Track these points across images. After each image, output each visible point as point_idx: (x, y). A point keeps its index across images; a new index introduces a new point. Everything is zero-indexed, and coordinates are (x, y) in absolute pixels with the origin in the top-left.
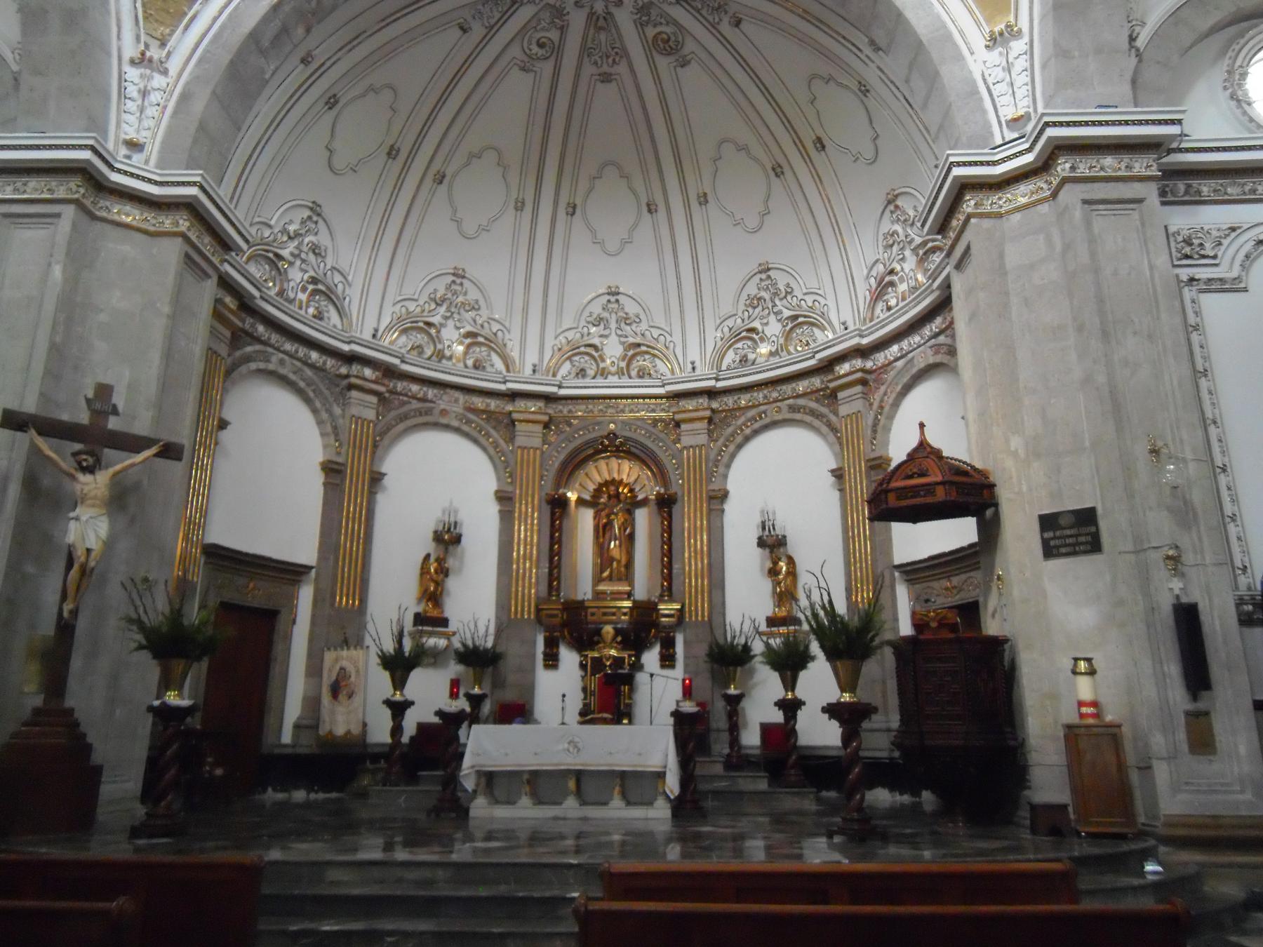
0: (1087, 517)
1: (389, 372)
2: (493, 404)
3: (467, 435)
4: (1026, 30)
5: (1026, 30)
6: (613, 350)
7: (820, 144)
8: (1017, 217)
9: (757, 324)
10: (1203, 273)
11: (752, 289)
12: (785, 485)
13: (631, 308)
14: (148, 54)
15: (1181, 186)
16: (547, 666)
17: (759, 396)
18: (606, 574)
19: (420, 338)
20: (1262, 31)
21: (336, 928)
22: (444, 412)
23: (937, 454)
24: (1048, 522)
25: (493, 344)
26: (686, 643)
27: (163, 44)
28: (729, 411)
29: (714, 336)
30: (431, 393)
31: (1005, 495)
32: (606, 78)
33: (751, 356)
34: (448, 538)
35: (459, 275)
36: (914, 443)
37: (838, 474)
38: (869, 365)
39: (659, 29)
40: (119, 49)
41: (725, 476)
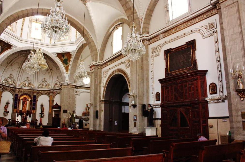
0: (66, 110)
1: (3, 86)
2: (13, 89)
3: (10, 92)
6: (27, 84)
7: (52, 70)
8: (65, 88)
9: (43, 84)
10: (77, 94)
11: (43, 80)
12: (43, 100)
13: (29, 79)
15: (77, 87)
16: (17, 117)
17: (42, 91)
18: (24, 108)
19: (6, 81)
22: (8, 90)
23: (57, 104)
24: (64, 110)
25: (14, 82)
26: (32, 115)
28: (40, 92)
29: (38, 84)
30: (7, 87)
31: (62, 108)
33: (42, 87)
34: (8, 103)
35: (11, 74)
36: (56, 103)
37: (49, 101)
38: (54, 91)
41: (38, 99)
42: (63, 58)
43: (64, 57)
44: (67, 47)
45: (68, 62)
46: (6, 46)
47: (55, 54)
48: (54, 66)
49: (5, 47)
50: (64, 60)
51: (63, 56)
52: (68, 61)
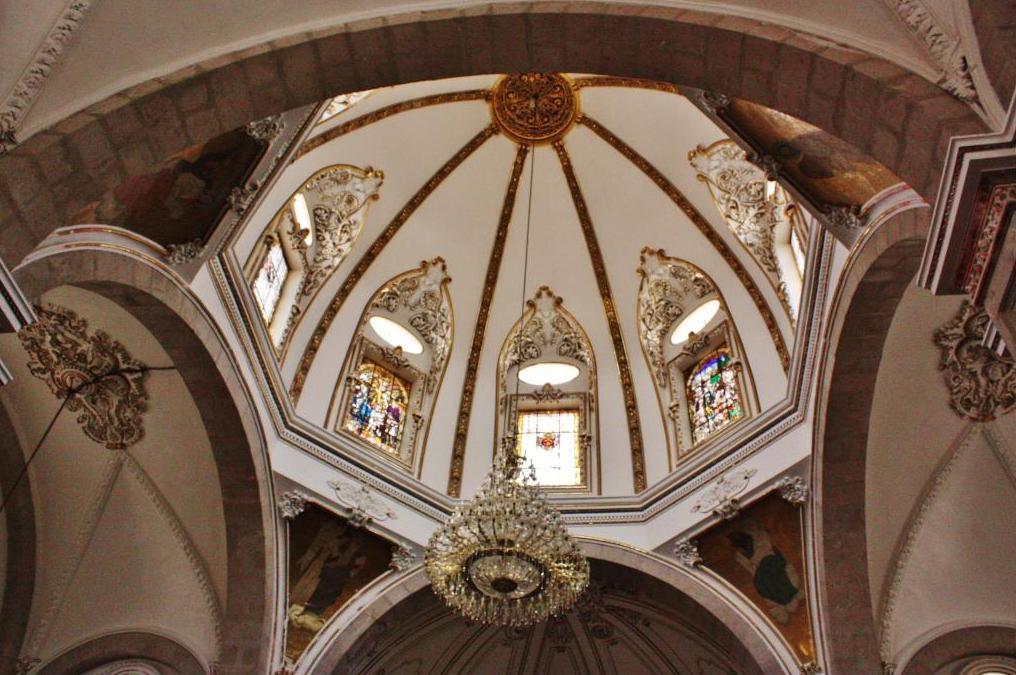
4: (823, 667)
5: (823, 667)
14: (287, 669)
20: (1008, 663)
21: (789, 118)
27: (295, 662)
32: (561, 650)
39: (596, 624)
40: (271, 667)
42: (743, 561)
43: (749, 554)
44: (748, 465)
45: (794, 580)
46: (358, 555)
47: (687, 551)
48: (710, 662)
49: (353, 560)
50: (759, 569)
51: (745, 544)
52: (789, 569)
